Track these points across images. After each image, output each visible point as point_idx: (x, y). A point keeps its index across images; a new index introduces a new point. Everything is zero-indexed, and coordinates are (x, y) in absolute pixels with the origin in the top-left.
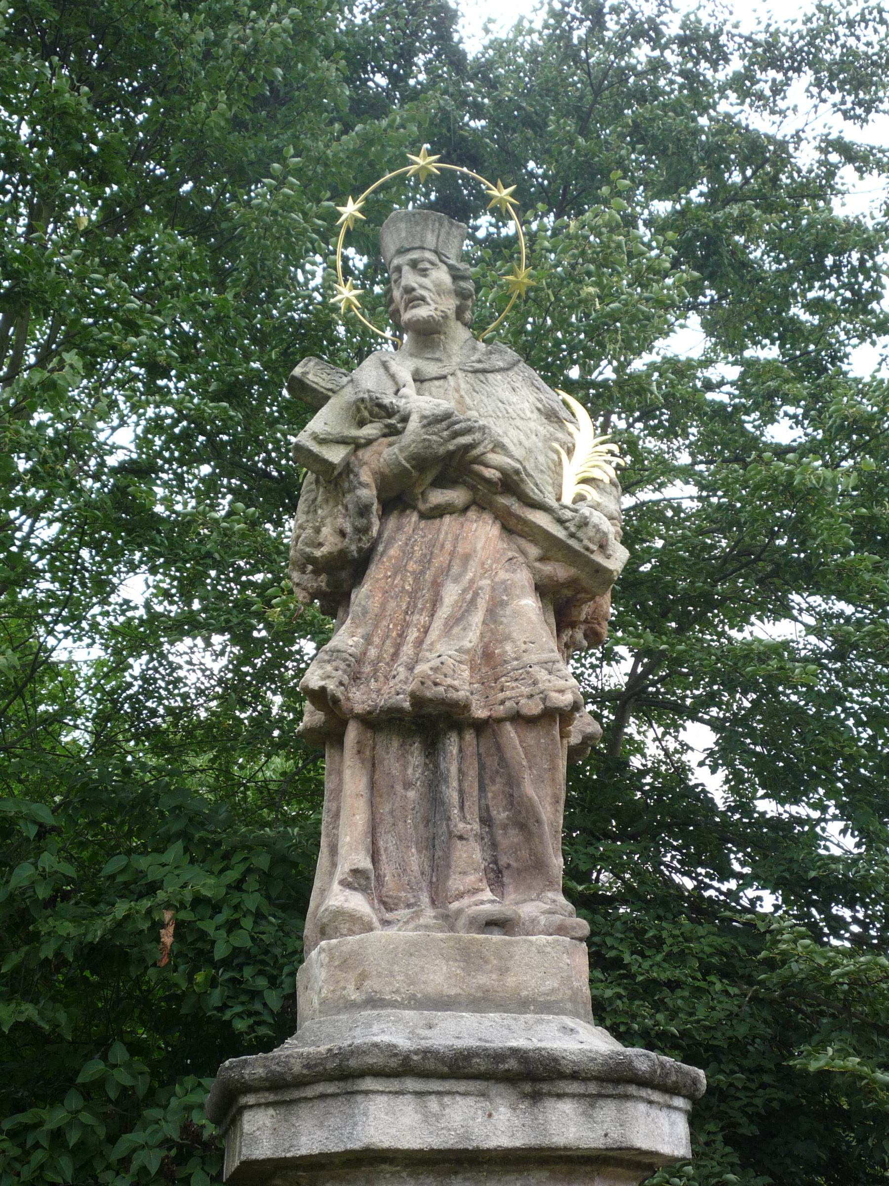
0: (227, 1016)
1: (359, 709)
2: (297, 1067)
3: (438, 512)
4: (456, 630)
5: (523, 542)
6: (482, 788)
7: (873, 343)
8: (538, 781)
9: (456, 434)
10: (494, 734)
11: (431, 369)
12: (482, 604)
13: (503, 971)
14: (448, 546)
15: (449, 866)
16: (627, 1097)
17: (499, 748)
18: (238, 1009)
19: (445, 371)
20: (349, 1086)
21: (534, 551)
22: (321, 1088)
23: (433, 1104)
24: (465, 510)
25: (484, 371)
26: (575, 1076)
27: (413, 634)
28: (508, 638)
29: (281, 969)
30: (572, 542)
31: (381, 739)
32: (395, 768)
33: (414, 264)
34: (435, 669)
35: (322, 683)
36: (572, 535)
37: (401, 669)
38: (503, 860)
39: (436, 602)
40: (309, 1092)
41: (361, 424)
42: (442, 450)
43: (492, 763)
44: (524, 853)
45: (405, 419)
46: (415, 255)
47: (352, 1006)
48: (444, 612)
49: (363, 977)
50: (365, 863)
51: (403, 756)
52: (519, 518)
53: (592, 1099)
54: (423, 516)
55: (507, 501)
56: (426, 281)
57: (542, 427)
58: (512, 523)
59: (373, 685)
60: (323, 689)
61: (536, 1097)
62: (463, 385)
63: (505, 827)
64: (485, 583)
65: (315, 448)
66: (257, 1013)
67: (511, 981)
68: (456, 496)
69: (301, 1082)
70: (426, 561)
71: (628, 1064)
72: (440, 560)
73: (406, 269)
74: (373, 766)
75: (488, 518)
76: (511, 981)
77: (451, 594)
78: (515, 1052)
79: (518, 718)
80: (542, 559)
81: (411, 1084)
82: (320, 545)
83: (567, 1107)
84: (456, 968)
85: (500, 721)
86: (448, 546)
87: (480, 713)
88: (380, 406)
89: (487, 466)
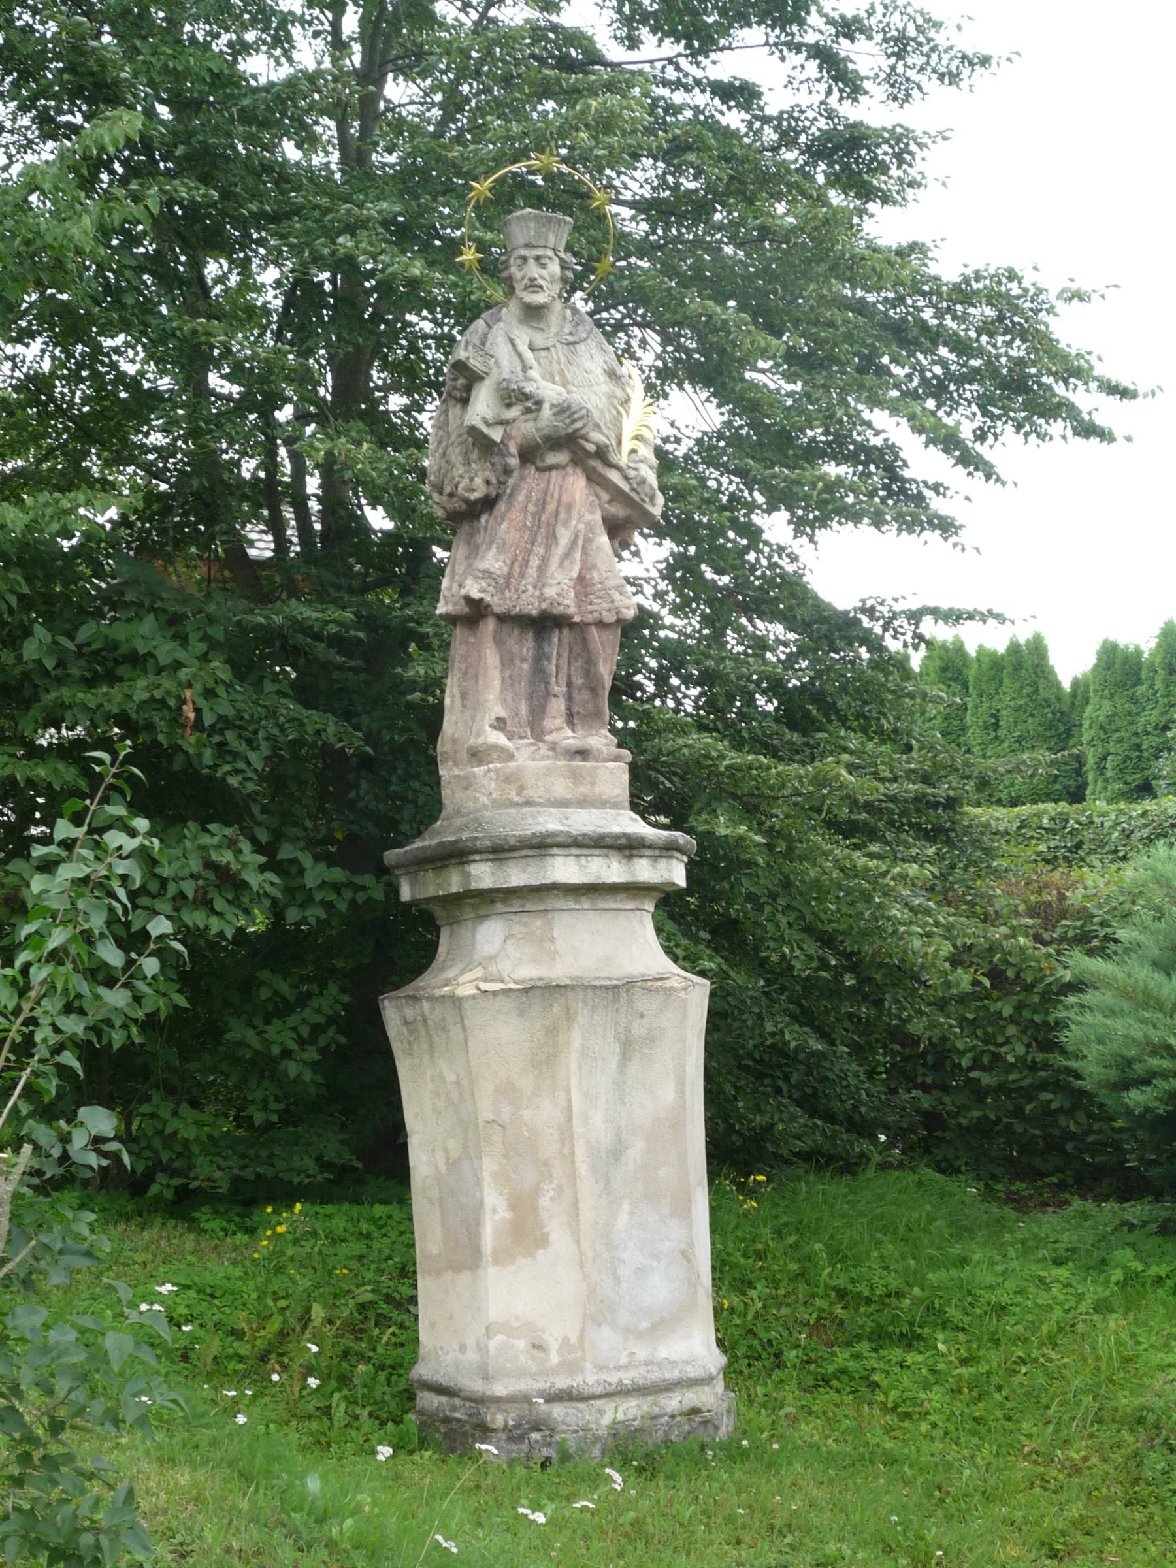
2: (512, 842)
3: (551, 468)
4: (566, 563)
5: (599, 489)
6: (569, 665)
7: (783, 59)
8: (605, 661)
9: (574, 421)
10: (582, 631)
11: (540, 341)
12: (580, 543)
13: (593, 784)
14: (556, 496)
15: (544, 712)
16: (672, 857)
17: (584, 641)
18: (227, 768)
19: (549, 343)
20: (543, 851)
21: (605, 496)
22: (524, 852)
23: (583, 860)
24: (564, 467)
25: (574, 343)
26: (650, 847)
27: (535, 562)
28: (595, 567)
30: (633, 494)
31: (506, 628)
32: (515, 648)
33: (537, 258)
34: (559, 595)
35: (482, 595)
36: (633, 489)
37: (530, 587)
38: (575, 709)
40: (517, 854)
41: (509, 406)
42: (563, 433)
43: (578, 649)
44: (590, 706)
46: (540, 252)
49: (521, 789)
50: (503, 714)
51: (520, 641)
52: (600, 475)
53: (655, 858)
54: (538, 469)
56: (544, 272)
58: (594, 477)
59: (507, 594)
60: (482, 600)
61: (630, 857)
62: (563, 359)
63: (580, 689)
64: (582, 526)
65: (486, 430)
66: (242, 771)
67: (597, 790)
68: (561, 457)
69: (513, 849)
72: (551, 507)
73: (531, 262)
75: (579, 472)
76: (597, 790)
77: (564, 537)
78: (625, 835)
79: (601, 624)
80: (609, 502)
81: (574, 851)
82: (473, 490)
85: (587, 624)
86: (556, 496)
87: (577, 619)
88: (524, 394)
89: (587, 440)
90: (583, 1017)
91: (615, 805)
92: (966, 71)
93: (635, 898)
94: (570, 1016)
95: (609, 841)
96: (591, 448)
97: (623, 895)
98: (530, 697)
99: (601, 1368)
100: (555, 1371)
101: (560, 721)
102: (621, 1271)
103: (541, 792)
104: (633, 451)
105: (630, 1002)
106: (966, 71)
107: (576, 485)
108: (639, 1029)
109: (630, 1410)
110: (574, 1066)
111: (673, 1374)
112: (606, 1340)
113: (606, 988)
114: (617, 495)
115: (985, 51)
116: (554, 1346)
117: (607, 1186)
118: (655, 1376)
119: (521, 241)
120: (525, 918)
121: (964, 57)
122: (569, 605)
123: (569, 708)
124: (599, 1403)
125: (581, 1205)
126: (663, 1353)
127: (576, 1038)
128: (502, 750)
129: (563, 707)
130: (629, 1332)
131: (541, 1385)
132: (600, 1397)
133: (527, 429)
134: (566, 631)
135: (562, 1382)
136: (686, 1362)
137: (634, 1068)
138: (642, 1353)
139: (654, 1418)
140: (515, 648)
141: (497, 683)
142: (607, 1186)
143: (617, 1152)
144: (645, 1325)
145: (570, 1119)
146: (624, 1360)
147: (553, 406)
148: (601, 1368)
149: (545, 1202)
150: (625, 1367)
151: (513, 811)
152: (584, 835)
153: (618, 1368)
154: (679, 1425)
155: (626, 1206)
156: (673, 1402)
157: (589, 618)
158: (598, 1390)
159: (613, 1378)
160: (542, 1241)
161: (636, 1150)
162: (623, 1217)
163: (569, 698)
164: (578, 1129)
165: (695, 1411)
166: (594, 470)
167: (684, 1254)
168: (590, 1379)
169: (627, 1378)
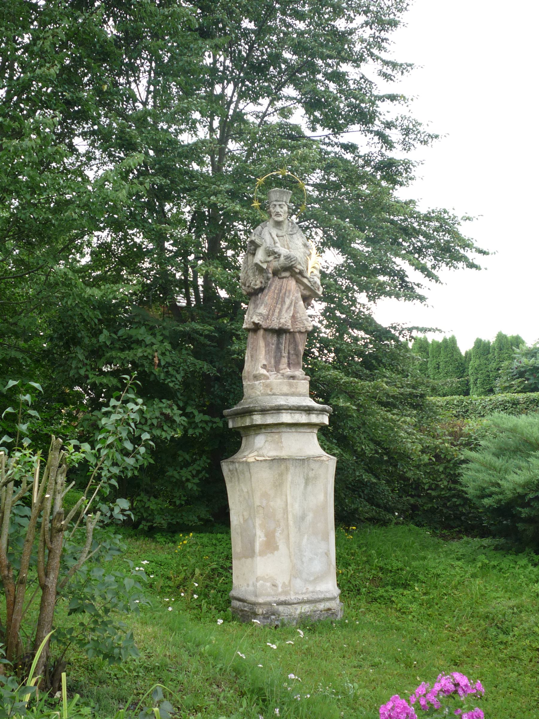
0: (166, 382)
1: (264, 327)
3: (283, 278)
7: (366, 136)
11: (280, 234)
13: (296, 388)
17: (294, 338)
18: (169, 380)
21: (302, 288)
27: (277, 310)
28: (298, 312)
29: (179, 368)
32: (270, 340)
33: (280, 205)
38: (291, 362)
39: (283, 302)
41: (269, 256)
43: (292, 340)
45: (280, 255)
46: (280, 203)
47: (270, 395)
48: (286, 306)
49: (271, 389)
50: (265, 363)
51: (272, 338)
53: (318, 414)
54: (279, 278)
55: (299, 276)
56: (282, 210)
57: (303, 249)
61: (309, 414)
65: (261, 264)
67: (298, 390)
68: (287, 274)
69: (268, 410)
70: (280, 290)
71: (325, 408)
72: (283, 291)
74: (264, 338)
75: (293, 279)
76: (298, 390)
77: (288, 302)
78: (307, 406)
79: (300, 332)
80: (304, 289)
81: (290, 411)
83: (314, 416)
84: (288, 387)
87: (292, 330)
90: (292, 470)
91: (304, 396)
92: (430, 140)
93: (311, 428)
94: (287, 469)
95: (302, 408)
96: (297, 271)
97: (306, 427)
98: (275, 357)
99: (296, 593)
100: (280, 594)
101: (285, 366)
102: (304, 559)
103: (278, 390)
104: (312, 272)
105: (308, 465)
106: (430, 140)
107: (292, 283)
108: (311, 474)
109: (306, 608)
110: (288, 486)
111: (321, 596)
112: (298, 584)
113: (300, 460)
114: (306, 287)
115: (437, 133)
116: (280, 585)
117: (299, 529)
118: (315, 597)
119: (274, 199)
120: (272, 434)
121: (429, 135)
122: (289, 326)
123: (288, 361)
124: (295, 606)
125: (290, 536)
126: (318, 589)
127: (289, 477)
128: (265, 375)
129: (286, 361)
130: (306, 581)
131: (275, 599)
132: (296, 604)
133: (275, 264)
134: (288, 335)
135: (283, 598)
136: (326, 592)
137: (310, 487)
138: (311, 589)
139: (315, 612)
140: (270, 340)
141: (264, 352)
142: (299, 529)
143: (303, 518)
144: (312, 578)
145: (287, 505)
146: (304, 591)
147: (284, 256)
148: (296, 593)
149: (277, 534)
150: (305, 593)
151: (268, 397)
152: (293, 406)
153: (302, 594)
154: (324, 614)
155: (306, 537)
156: (322, 606)
157: (296, 330)
158: (295, 601)
159: (300, 597)
160: (276, 548)
161: (310, 517)
162: (305, 540)
163: (289, 358)
164: (289, 509)
165: (329, 609)
166: (298, 279)
167: (326, 554)
168: (292, 597)
169: (305, 597)
